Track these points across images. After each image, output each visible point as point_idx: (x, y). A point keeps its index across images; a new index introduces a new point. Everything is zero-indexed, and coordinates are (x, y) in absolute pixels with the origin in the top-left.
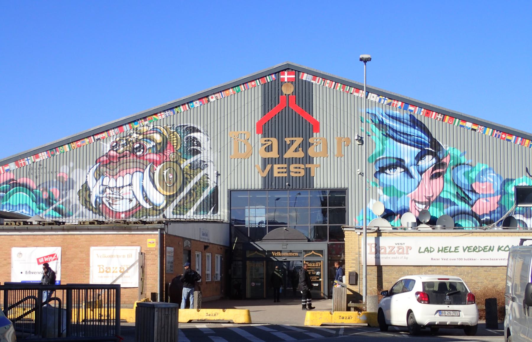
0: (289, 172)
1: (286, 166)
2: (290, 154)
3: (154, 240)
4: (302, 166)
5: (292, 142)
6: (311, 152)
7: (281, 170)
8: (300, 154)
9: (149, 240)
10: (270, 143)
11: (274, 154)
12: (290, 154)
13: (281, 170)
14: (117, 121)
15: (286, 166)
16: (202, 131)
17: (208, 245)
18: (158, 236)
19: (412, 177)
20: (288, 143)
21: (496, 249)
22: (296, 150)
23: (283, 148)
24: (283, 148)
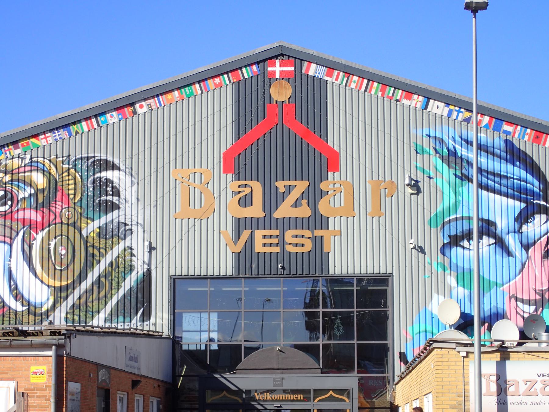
0: (283, 243)
1: (277, 232)
2: (284, 211)
4: (308, 233)
5: (289, 189)
6: (323, 207)
8: (304, 211)
9: (33, 369)
10: (247, 190)
11: (256, 211)
12: (284, 211)
15: (332, 237)
22: (296, 204)
23: (272, 200)
24: (272, 200)
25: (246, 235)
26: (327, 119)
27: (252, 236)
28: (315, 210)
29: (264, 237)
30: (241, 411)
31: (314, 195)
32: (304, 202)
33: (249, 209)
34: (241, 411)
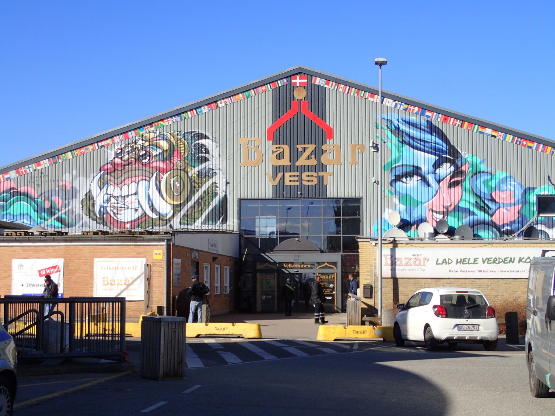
1: (298, 174)
2: (302, 161)
3: (161, 251)
4: (315, 174)
5: (305, 149)
7: (292, 179)
8: (313, 162)
9: (155, 251)
10: (281, 150)
11: (286, 161)
12: (302, 161)
13: (292, 179)
15: (298, 174)
20: (300, 150)
21: (517, 260)
22: (308, 158)
23: (295, 155)
24: (295, 155)
27: (283, 175)
28: (319, 161)
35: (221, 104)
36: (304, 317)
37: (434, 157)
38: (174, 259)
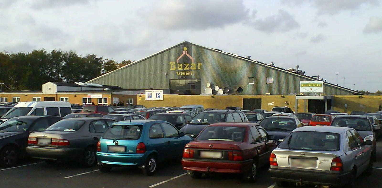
0: (185, 74)
1: (184, 72)
2: (185, 69)
3: (110, 96)
4: (189, 72)
5: (186, 65)
6: (191, 68)
7: (183, 73)
8: (188, 69)
9: (109, 96)
10: (180, 65)
11: (181, 69)
12: (185, 69)
13: (183, 73)
14: (143, 59)
15: (184, 72)
16: (223, 95)
17: (124, 95)
18: (83, 87)
19: (291, 136)
20: (185, 65)
21: (236, 90)
22: (187, 68)
23: (184, 67)
24: (184, 67)
25: (180, 72)
26: (146, 59)
27: (181, 72)
28: (190, 68)
29: (183, 73)
30: (381, 122)
31: (190, 66)
32: (189, 67)
33: (173, 69)
34: (381, 122)
35: (232, 54)
36: (33, 151)
37: (162, 132)
38: (45, 115)
